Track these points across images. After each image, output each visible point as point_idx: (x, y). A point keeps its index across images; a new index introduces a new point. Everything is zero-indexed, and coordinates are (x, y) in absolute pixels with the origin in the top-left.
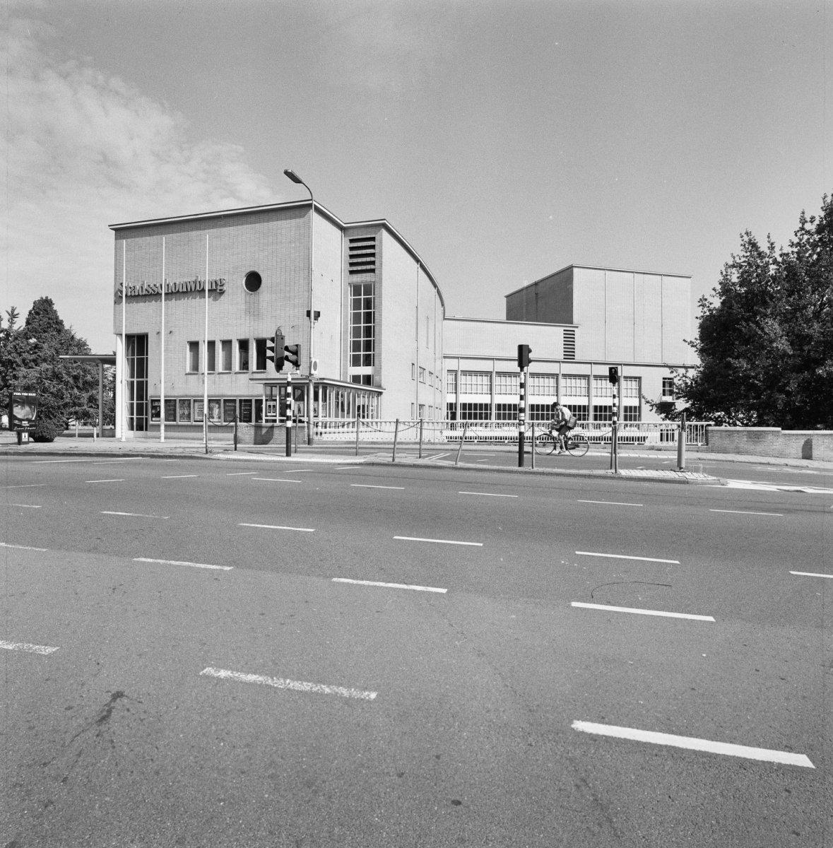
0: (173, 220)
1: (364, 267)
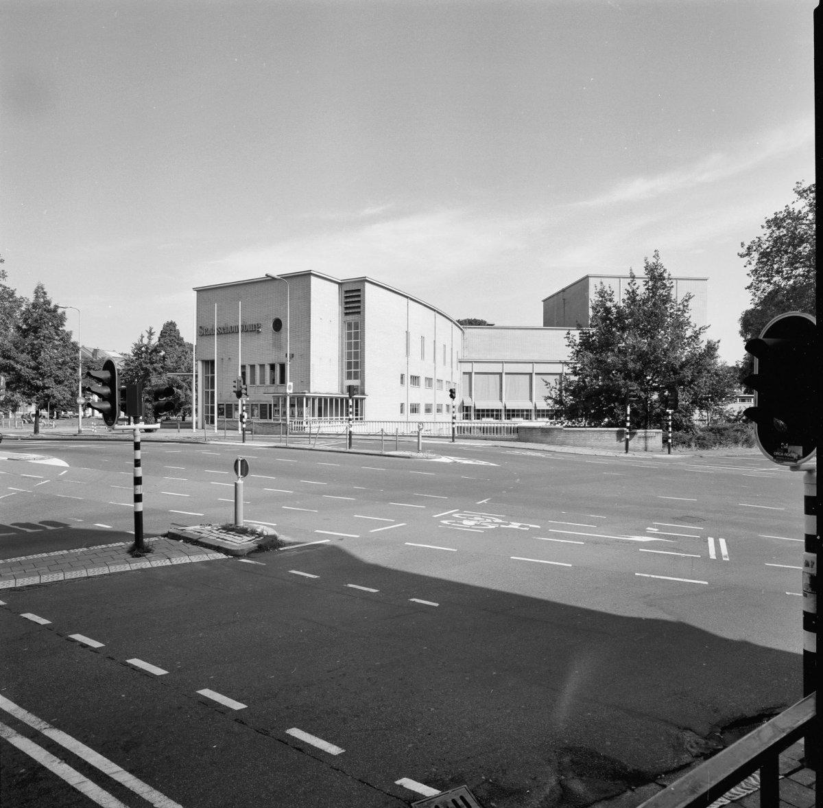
1: (354, 311)
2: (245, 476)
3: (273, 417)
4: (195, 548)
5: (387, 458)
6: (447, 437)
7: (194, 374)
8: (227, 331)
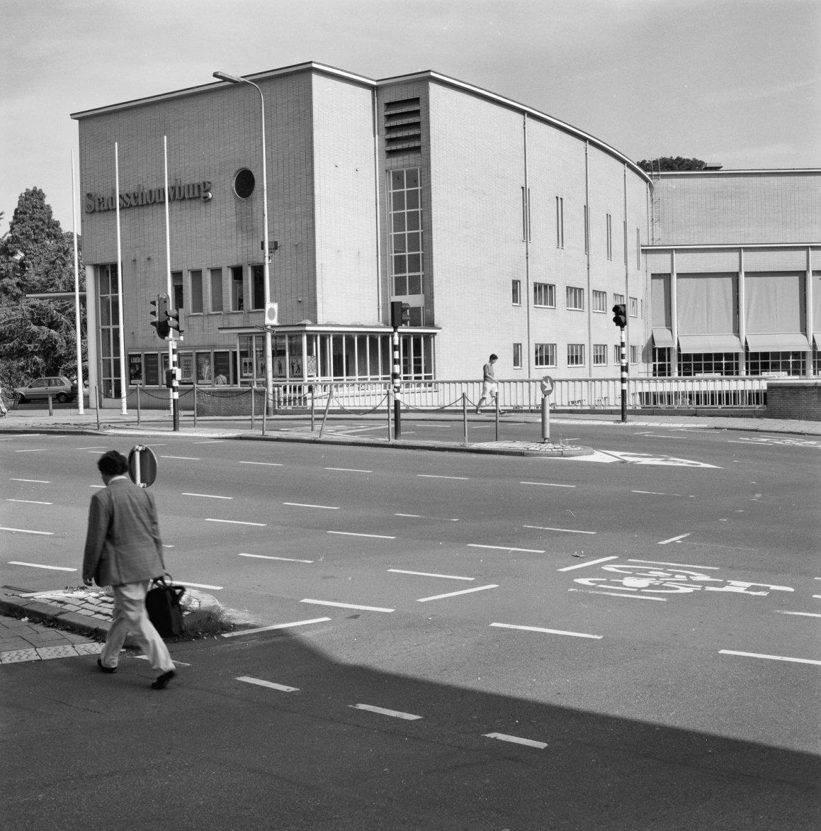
1: (405, 145)
2: (149, 484)
3: (239, 380)
4: (52, 633)
5: (474, 456)
6: (611, 412)
7: (77, 294)
8: (141, 201)
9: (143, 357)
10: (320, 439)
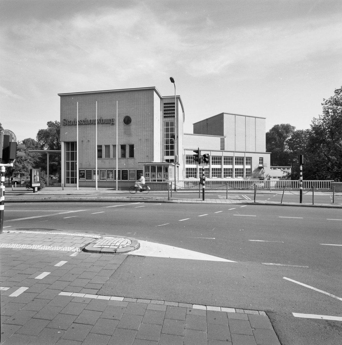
0: (86, 93)
9: (85, 171)
10: (313, 205)
